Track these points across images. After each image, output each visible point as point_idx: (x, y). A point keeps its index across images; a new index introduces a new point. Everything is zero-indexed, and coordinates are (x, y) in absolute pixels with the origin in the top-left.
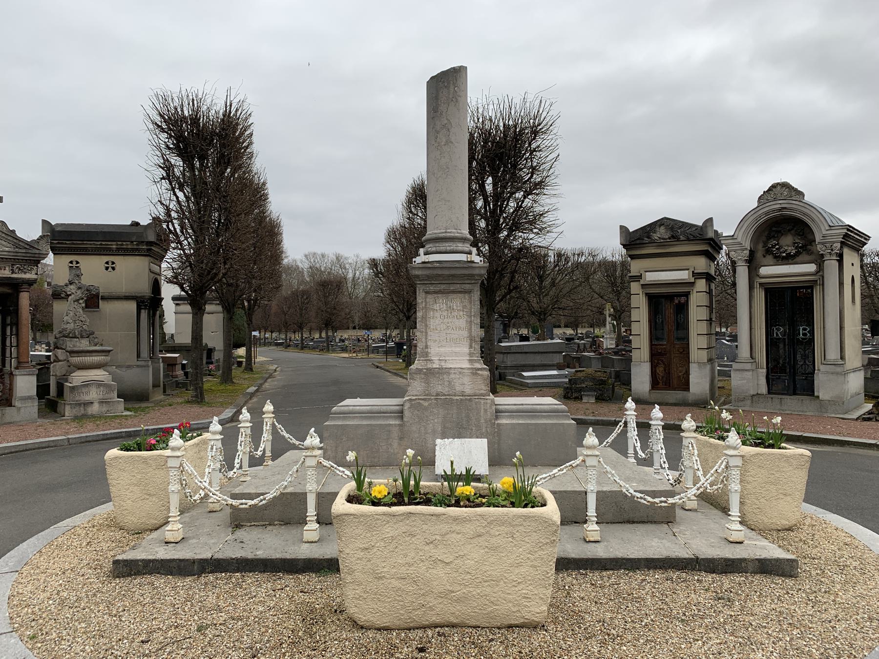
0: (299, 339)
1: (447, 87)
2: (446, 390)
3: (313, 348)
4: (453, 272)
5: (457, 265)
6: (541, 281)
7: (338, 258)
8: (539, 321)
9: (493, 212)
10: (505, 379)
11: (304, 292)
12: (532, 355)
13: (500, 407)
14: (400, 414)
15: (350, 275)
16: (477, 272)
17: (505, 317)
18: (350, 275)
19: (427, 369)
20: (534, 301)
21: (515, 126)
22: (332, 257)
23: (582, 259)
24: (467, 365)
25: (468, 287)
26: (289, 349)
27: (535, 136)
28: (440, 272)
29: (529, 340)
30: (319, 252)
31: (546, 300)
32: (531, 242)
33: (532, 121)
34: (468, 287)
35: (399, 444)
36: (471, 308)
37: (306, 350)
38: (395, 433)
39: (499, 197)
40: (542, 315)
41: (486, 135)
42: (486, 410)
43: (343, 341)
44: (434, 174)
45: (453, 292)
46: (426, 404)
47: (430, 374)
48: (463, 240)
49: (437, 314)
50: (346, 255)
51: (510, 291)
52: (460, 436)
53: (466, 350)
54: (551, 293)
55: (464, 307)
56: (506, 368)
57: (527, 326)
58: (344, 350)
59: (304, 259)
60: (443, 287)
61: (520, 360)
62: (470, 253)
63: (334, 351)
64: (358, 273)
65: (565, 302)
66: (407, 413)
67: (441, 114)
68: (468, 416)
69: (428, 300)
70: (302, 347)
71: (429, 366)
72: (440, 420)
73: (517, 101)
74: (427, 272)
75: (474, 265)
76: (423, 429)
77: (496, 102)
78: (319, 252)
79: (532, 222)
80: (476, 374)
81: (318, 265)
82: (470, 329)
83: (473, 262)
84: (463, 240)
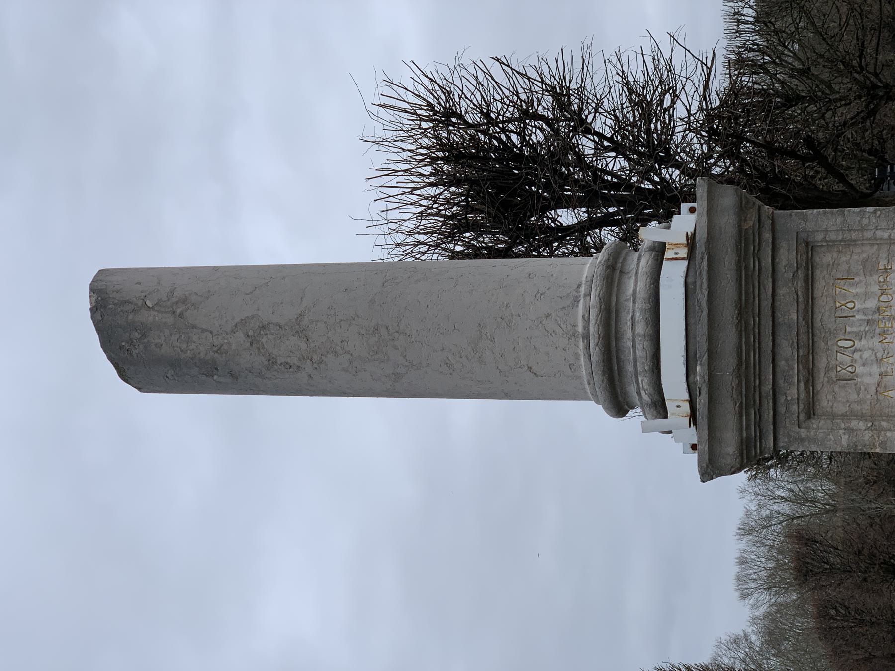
1: (145, 330)
5: (702, 296)
6: (798, 99)
9: (628, 204)
11: (824, 613)
16: (727, 222)
17: (882, 172)
20: (844, 113)
21: (434, 160)
22: (744, 543)
25: (787, 256)
27: (454, 114)
28: (728, 362)
30: (736, 569)
31: (843, 85)
33: (424, 125)
34: (787, 256)
36: (875, 241)
39: (595, 191)
41: (456, 227)
44: (397, 377)
48: (613, 274)
50: (741, 514)
54: (826, 76)
55: (869, 267)
60: (786, 350)
62: (659, 249)
64: (779, 492)
65: (848, 44)
67: (219, 350)
69: (841, 408)
73: (381, 158)
74: (729, 408)
75: (702, 236)
77: (382, 205)
78: (735, 570)
81: (764, 574)
83: (691, 241)
84: (613, 274)
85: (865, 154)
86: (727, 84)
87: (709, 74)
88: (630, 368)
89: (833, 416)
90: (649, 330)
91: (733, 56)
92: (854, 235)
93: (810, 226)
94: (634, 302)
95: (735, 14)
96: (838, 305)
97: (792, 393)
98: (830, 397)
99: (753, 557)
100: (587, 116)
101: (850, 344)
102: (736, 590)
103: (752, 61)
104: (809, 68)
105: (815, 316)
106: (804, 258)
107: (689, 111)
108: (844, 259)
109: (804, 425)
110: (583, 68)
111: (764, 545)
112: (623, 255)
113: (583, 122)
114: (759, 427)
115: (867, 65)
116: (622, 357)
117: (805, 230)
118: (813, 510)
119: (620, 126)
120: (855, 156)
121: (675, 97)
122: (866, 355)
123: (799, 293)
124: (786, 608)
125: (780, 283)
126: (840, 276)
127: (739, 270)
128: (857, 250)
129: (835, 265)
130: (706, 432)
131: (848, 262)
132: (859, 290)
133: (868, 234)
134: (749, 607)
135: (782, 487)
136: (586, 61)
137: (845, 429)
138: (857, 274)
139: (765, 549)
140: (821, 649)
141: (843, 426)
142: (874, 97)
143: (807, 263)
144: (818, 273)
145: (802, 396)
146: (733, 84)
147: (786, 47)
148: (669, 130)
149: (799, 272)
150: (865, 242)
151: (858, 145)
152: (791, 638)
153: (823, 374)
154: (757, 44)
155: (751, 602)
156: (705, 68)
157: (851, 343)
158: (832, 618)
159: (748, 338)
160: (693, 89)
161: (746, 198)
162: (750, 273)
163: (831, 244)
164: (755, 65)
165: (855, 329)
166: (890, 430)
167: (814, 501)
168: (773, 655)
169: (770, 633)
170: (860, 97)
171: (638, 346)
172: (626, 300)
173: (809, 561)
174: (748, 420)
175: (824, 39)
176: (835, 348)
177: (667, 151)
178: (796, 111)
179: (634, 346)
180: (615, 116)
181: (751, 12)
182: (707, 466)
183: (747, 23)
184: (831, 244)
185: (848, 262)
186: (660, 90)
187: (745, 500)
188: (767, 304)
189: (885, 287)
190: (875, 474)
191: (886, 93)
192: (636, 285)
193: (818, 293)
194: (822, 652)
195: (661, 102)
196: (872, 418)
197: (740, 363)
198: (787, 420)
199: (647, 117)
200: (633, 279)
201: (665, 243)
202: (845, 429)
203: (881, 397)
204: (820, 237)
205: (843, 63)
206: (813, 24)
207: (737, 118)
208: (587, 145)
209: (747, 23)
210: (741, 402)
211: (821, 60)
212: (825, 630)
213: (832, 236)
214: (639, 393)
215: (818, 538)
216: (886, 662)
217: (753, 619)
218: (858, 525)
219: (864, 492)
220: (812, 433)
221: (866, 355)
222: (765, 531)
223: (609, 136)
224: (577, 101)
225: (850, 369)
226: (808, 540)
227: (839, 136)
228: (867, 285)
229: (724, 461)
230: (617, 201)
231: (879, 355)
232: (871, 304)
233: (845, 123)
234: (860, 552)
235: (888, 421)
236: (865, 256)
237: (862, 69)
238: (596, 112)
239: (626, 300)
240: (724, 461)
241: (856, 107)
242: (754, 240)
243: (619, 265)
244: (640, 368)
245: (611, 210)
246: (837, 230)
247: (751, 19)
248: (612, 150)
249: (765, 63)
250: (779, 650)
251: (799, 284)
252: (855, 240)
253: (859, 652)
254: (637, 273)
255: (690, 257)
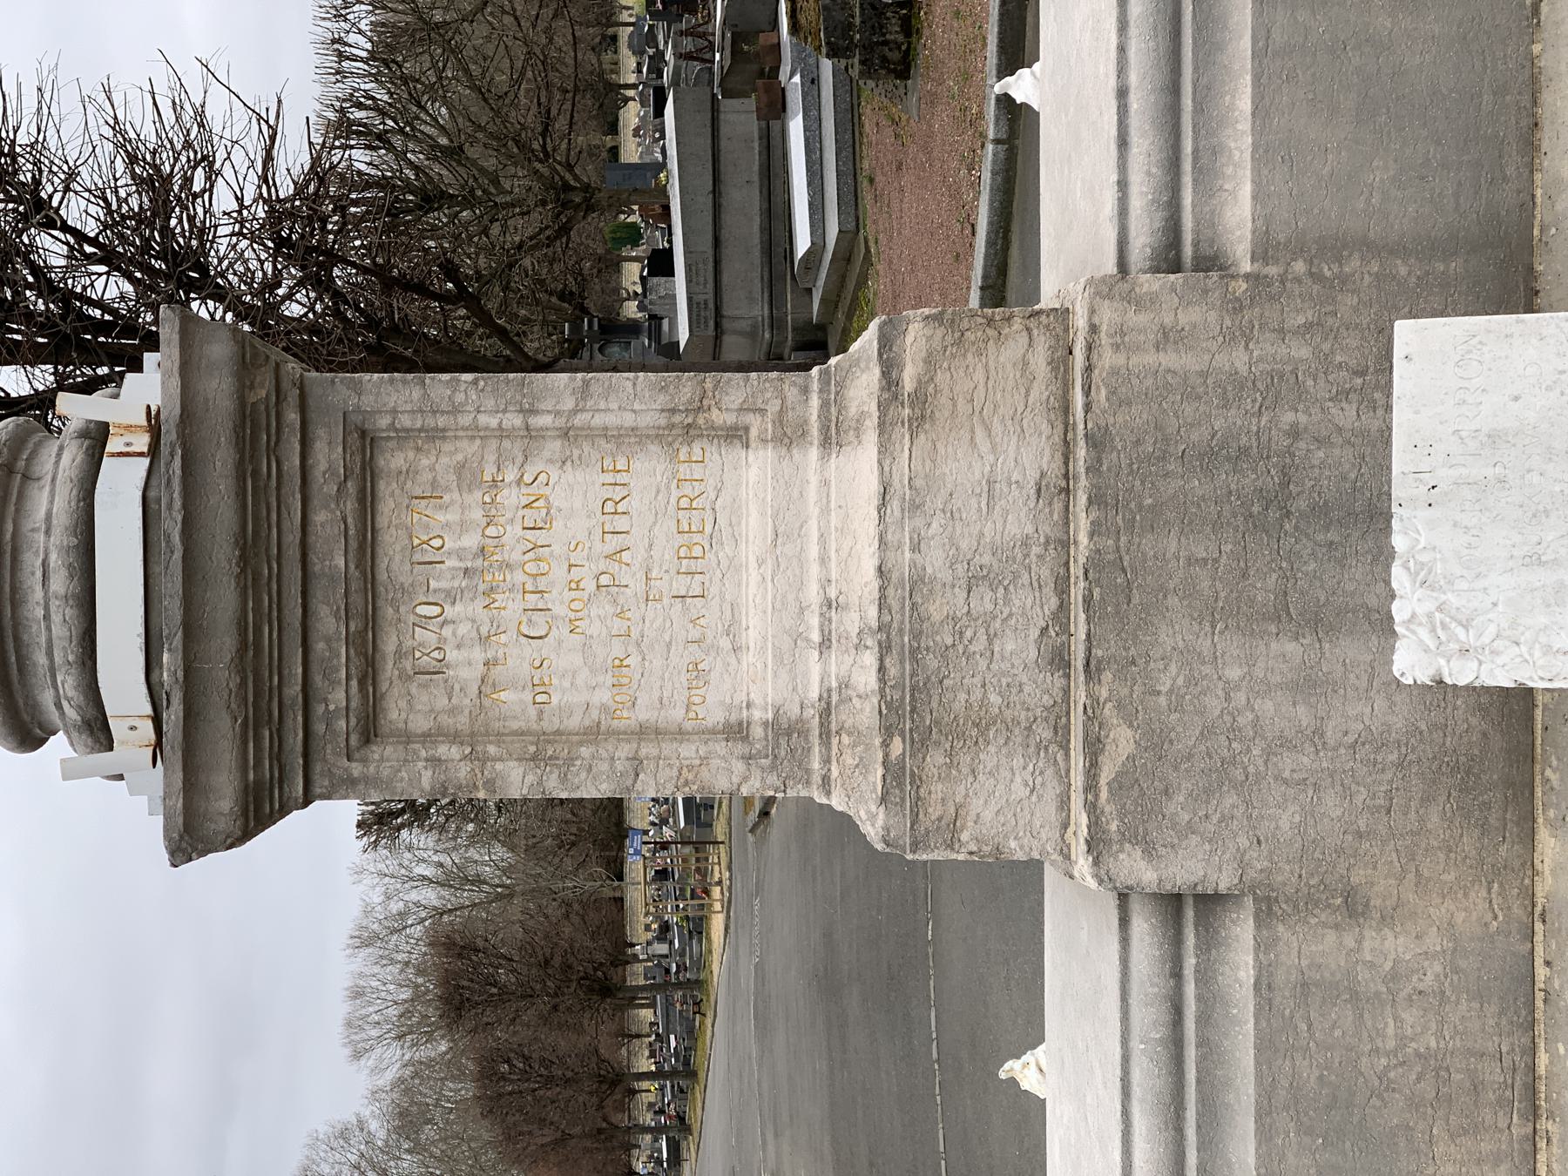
0: (653, 1086)
2: (1030, 606)
3: (691, 1035)
4: (221, 554)
5: (172, 525)
7: (365, 940)
8: (590, 208)
10: (822, 328)
11: (488, 1074)
12: (727, 219)
13: (1142, 241)
14: (1186, 912)
15: (430, 896)
16: (218, 389)
17: (576, 328)
18: (430, 896)
19: (888, 732)
20: (522, 228)
23: (360, 44)
24: (860, 466)
26: (693, 1118)
28: (222, 645)
29: (669, 253)
31: (517, 182)
32: (249, 195)
34: (328, 455)
35: (1386, 920)
36: (476, 432)
37: (698, 1060)
38: (1317, 946)
40: (571, 200)
42: (1167, 338)
43: (665, 928)
45: (366, 545)
46: (1122, 742)
47: (919, 715)
49: (518, 659)
51: (474, 303)
52: (1366, 514)
53: (753, 472)
54: (490, 163)
55: (466, 476)
56: (776, 323)
57: (613, 265)
58: (697, 928)
59: (369, 1061)
60: (328, 622)
61: (745, 266)
62: (97, 436)
63: (701, 963)
64: (421, 870)
66: (1187, 869)
68: (1208, 458)
69: (420, 724)
70: (683, 1073)
71: (864, 714)
72: (1231, 645)
74: (222, 731)
76: (1287, 763)
79: (154, 183)
80: (920, 399)
81: (393, 1012)
82: (625, 439)
83: (154, 424)
85: (554, 299)
86: (305, 159)
87: (273, 138)
88: (41, 659)
89: (406, 738)
90: (75, 587)
91: (331, 115)
92: (441, 421)
93: (368, 402)
94: (48, 532)
95: (334, 41)
96: (416, 542)
97: (338, 697)
98: (403, 704)
99: (374, 984)
100: (50, 197)
101: (436, 610)
102: (345, 1045)
103: (365, 125)
104: (461, 148)
105: (378, 561)
106: (358, 459)
107: (240, 200)
108: (425, 462)
109: (357, 756)
110: (39, 109)
111: (393, 962)
112: (30, 445)
113: (40, 205)
114: (279, 761)
115: (554, 150)
116: (25, 637)
117: (358, 410)
118: (478, 897)
119: (113, 221)
120: (538, 302)
121: (212, 175)
122: (464, 629)
123: (350, 520)
124: (429, 1067)
125: (315, 502)
126: (419, 492)
127: (241, 478)
128: (447, 447)
129: (410, 472)
130: (181, 775)
131: (432, 469)
132: (451, 516)
133: (465, 420)
134: (367, 1071)
135: (424, 861)
136: (47, 96)
137: (427, 760)
138: (447, 489)
139: (396, 969)
140: (485, 1132)
141: (423, 754)
142: (565, 205)
143: (363, 469)
144: (382, 485)
145: (354, 704)
146: (316, 161)
147: (423, 108)
148: (202, 232)
149: (349, 484)
150: (461, 433)
151: (542, 282)
152: (438, 1119)
153: (391, 664)
154: (373, 98)
155: (371, 1062)
156: (264, 127)
157: (437, 610)
158: (503, 1078)
159: (258, 601)
160: (247, 163)
161: (253, 346)
162: (262, 484)
163: (404, 436)
164: (370, 133)
165: (444, 584)
166: (501, 759)
167: (479, 881)
168: (408, 1151)
169: (403, 1114)
170: (544, 203)
171: (53, 617)
172: (33, 530)
173: (465, 983)
174: (258, 749)
175: (485, 100)
176: (412, 619)
177: (203, 269)
178: (439, 218)
179: (47, 617)
180: (105, 200)
181: (361, 41)
182: (181, 837)
183: (355, 59)
184: (404, 436)
185: (432, 469)
186: (184, 159)
187: (361, 887)
188: (292, 538)
189: (493, 512)
190: (574, 830)
191: (586, 200)
192: (52, 502)
193: (382, 521)
194: (486, 1136)
195: (188, 181)
196: (472, 739)
197: (243, 647)
198: (329, 746)
199: (162, 208)
200: (47, 488)
201: (107, 425)
202: (427, 760)
203: (487, 702)
204: (384, 422)
205: (517, 142)
206: (467, 71)
207: (324, 221)
208: (52, 249)
209: (355, 59)
210: (246, 717)
211: (480, 135)
212: (491, 1098)
213: (405, 421)
214: (59, 706)
215: (480, 943)
216: (588, 1144)
217: (374, 1093)
218: (547, 917)
219: (557, 860)
220: (372, 769)
221: (464, 629)
222: (395, 937)
223: (92, 235)
224: (30, 167)
225: (435, 654)
226: (463, 947)
227: (511, 266)
228: (463, 507)
229: (213, 826)
230: (108, 355)
231: (484, 630)
232: (471, 541)
233: (520, 247)
234: (547, 962)
235: (498, 744)
236: (460, 457)
237: (547, 155)
238: (67, 189)
239: (33, 530)
240: (213, 826)
241: (538, 219)
242: (268, 425)
243: (21, 464)
244: (58, 659)
245: (100, 371)
246: (413, 412)
247: (364, 54)
248: (100, 262)
249: (386, 132)
250: (417, 1142)
251: (349, 503)
252: (444, 430)
253: (546, 1131)
254: (54, 480)
255: (154, 451)
